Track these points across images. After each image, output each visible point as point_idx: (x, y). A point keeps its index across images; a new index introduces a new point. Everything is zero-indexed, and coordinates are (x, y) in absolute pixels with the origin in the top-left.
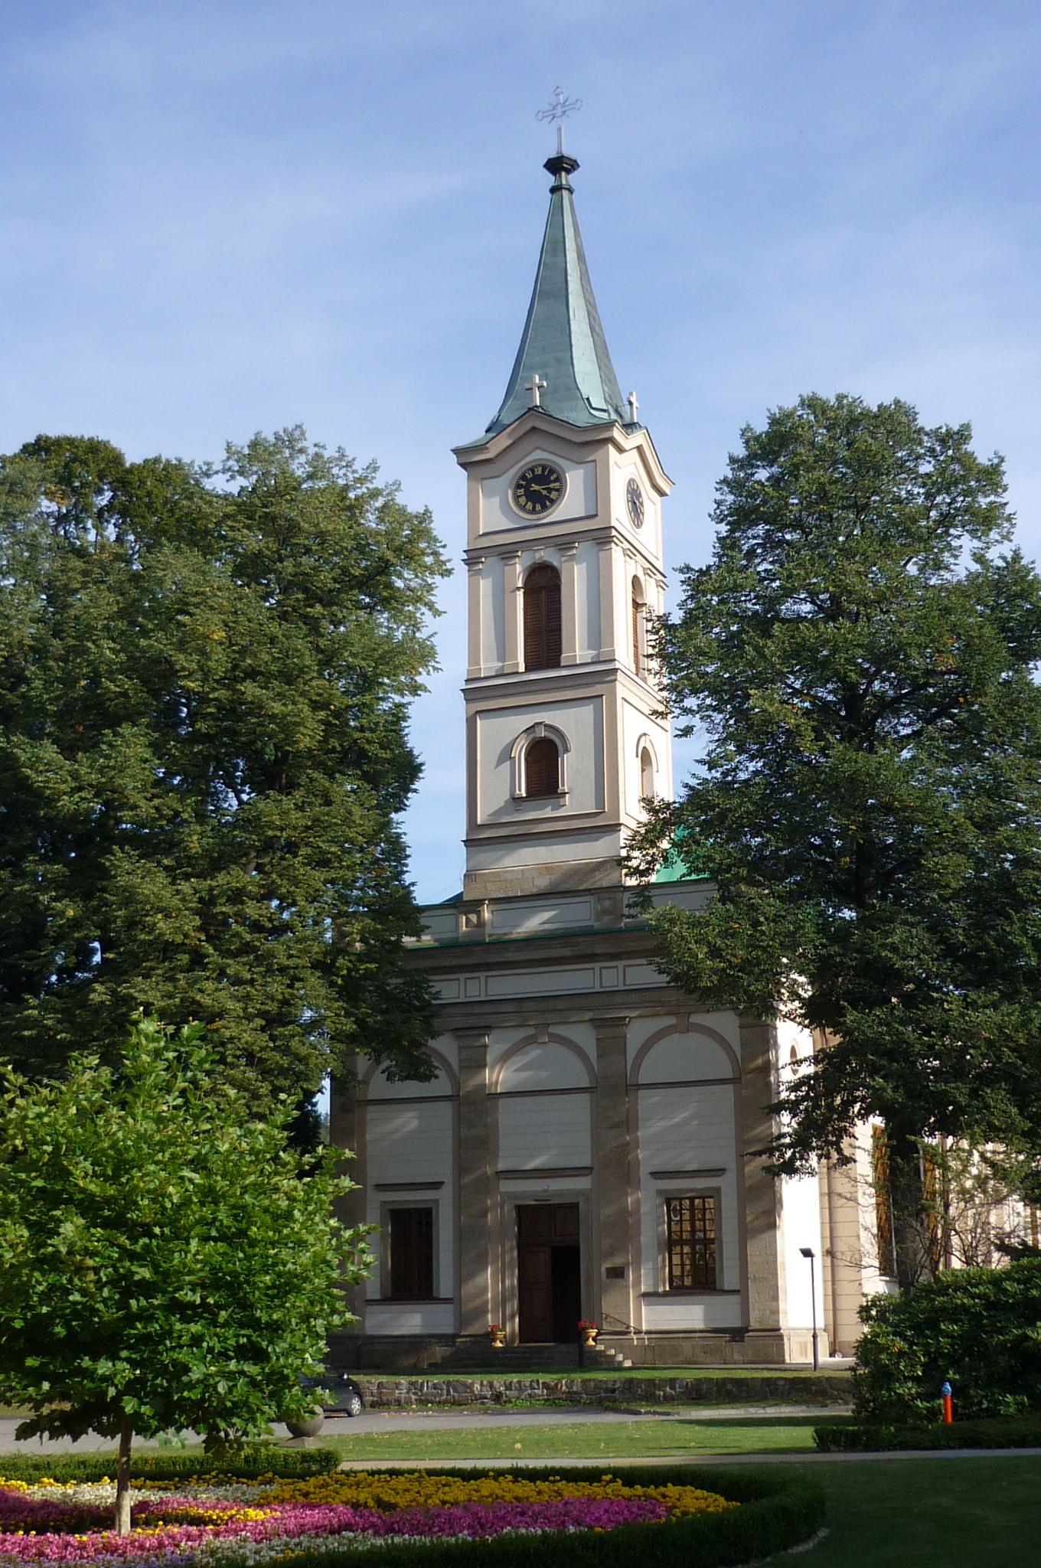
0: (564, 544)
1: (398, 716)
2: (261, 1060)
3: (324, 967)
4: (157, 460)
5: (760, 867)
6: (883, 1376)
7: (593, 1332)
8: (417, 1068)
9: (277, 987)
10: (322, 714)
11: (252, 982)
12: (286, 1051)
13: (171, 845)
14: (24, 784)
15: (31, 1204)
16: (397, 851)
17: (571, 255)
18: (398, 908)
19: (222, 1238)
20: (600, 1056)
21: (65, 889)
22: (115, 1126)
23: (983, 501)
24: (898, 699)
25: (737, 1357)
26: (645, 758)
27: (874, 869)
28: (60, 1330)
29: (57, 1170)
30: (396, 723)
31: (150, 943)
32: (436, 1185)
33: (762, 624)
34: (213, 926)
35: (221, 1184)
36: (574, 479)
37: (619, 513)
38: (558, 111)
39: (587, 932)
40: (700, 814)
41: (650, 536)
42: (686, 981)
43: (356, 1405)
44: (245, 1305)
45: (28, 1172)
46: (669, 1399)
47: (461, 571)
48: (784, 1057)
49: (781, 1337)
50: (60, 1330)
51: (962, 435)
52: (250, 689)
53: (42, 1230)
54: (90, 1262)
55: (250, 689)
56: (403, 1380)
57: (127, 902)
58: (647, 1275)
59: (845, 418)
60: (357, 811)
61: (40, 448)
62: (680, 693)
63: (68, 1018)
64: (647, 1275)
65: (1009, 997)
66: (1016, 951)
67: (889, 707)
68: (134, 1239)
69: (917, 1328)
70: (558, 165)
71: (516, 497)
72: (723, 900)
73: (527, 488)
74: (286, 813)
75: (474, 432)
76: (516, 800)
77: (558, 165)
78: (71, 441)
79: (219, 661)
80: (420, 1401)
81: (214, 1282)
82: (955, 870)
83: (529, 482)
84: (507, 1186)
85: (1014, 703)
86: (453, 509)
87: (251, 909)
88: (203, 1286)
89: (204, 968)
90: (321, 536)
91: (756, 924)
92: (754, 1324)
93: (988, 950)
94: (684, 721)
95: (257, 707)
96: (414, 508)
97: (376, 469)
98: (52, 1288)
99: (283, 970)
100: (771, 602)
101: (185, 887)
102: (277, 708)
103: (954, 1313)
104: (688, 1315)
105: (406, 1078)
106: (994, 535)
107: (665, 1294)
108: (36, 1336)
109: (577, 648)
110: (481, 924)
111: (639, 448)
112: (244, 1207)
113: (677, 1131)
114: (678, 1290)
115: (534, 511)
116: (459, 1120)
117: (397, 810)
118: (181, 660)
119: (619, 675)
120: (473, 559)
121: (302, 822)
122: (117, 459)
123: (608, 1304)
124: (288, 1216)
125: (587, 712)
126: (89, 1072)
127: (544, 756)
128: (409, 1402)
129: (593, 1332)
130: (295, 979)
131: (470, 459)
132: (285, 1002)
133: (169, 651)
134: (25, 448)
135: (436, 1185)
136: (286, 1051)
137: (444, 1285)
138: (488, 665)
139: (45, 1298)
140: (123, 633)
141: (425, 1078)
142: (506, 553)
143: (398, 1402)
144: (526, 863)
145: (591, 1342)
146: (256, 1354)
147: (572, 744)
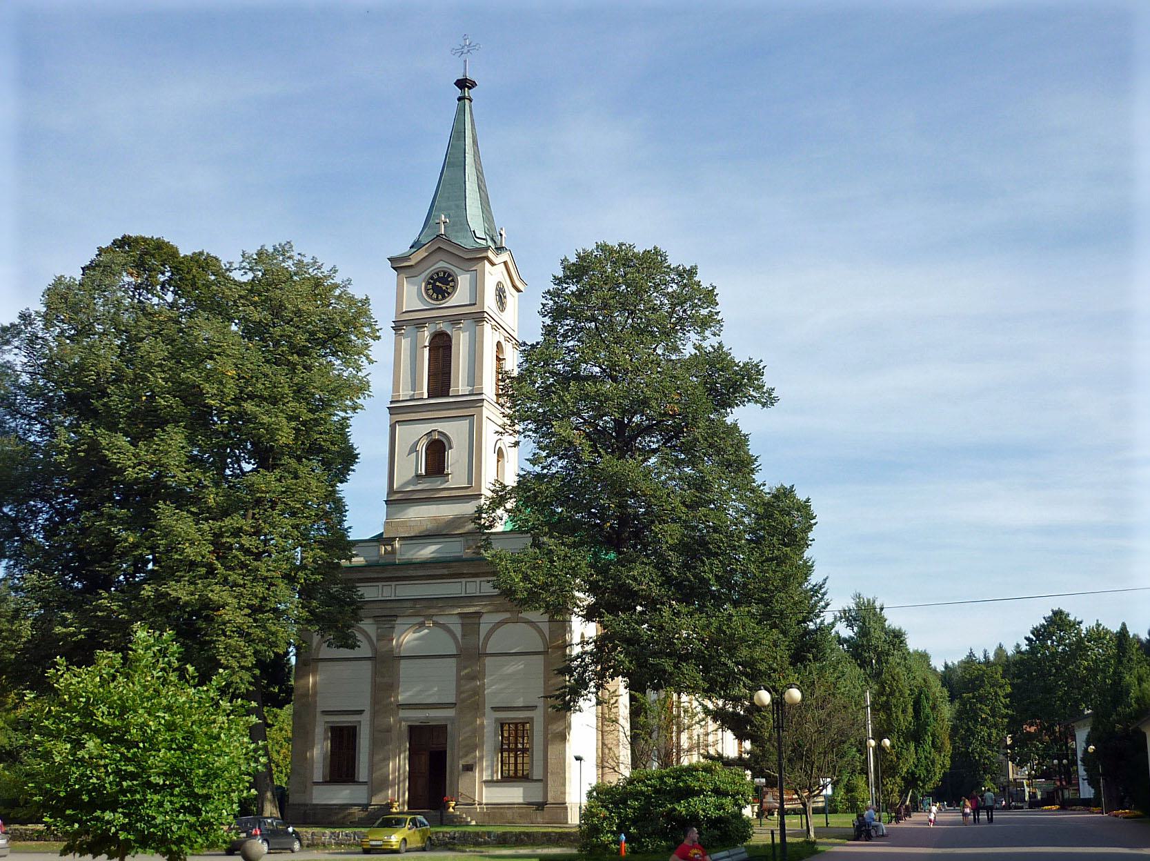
0: (455, 320)
1: (343, 425)
2: (249, 634)
3: (290, 578)
4: (201, 253)
5: (561, 527)
6: (594, 830)
7: (453, 804)
8: (347, 641)
9: (260, 589)
10: (293, 424)
11: (244, 586)
12: (264, 628)
13: (196, 500)
14: (104, 460)
15: (74, 730)
16: (339, 508)
17: (469, 141)
18: (339, 543)
19: (179, 748)
20: (463, 636)
21: (129, 525)
22: (120, 687)
23: (704, 312)
24: (650, 427)
25: (539, 820)
26: (500, 454)
27: (625, 532)
28: (85, 798)
29: (87, 713)
30: (343, 429)
31: (181, 561)
32: (360, 712)
33: (564, 379)
34: (221, 550)
35: (178, 719)
36: (463, 280)
37: (490, 302)
38: (463, 50)
39: (459, 560)
40: (528, 490)
41: (510, 317)
42: (508, 593)
43: (297, 846)
44: (189, 785)
45: (71, 712)
46: (486, 844)
47: (387, 334)
48: (576, 639)
49: (566, 808)
50: (85, 798)
51: (692, 272)
52: (249, 406)
53: (78, 744)
54: (102, 762)
55: (249, 406)
56: (327, 831)
57: (166, 536)
58: (487, 769)
59: (622, 257)
60: (314, 483)
61: (124, 243)
62: (512, 421)
63: (126, 605)
64: (487, 769)
65: (701, 610)
66: (704, 582)
67: (647, 430)
68: (128, 750)
69: (616, 804)
70: (463, 84)
71: (427, 290)
72: (534, 545)
73: (434, 285)
74: (269, 482)
75: (403, 248)
76: (418, 476)
77: (463, 84)
78: (144, 240)
79: (231, 389)
80: (336, 844)
81: (174, 772)
82: (670, 533)
83: (435, 281)
84: (403, 714)
85: (714, 434)
86: (383, 295)
87: (246, 541)
88: (165, 774)
89: (215, 576)
90: (298, 313)
91: (552, 561)
92: (550, 800)
93: (690, 581)
94: (517, 438)
95: (252, 419)
96: (359, 296)
97: (336, 271)
98: (82, 775)
99: (265, 579)
100: (575, 365)
101: (206, 527)
102: (266, 419)
103: (636, 795)
104: (514, 794)
105: (341, 646)
106: (707, 333)
107: (498, 781)
108: (72, 799)
109: (460, 385)
110: (393, 551)
111: (505, 263)
112: (192, 733)
113: (511, 682)
114: (509, 779)
115: (437, 299)
116: (376, 673)
117: (341, 482)
118: (206, 387)
119: (485, 403)
120: (398, 326)
121: (279, 489)
122: (174, 253)
123: (463, 784)
124: (218, 738)
125: (466, 423)
126: (107, 659)
127: (437, 450)
128: (330, 844)
129: (453, 804)
130: (271, 584)
131: (399, 264)
132: (264, 599)
133: (199, 381)
134: (115, 242)
135: (360, 712)
136: (264, 628)
137: (363, 773)
138: (405, 393)
139: (78, 780)
140: (170, 369)
141: (353, 647)
142: (419, 324)
143: (324, 844)
144: (421, 515)
145: (451, 810)
146: (197, 812)
147: (454, 444)
